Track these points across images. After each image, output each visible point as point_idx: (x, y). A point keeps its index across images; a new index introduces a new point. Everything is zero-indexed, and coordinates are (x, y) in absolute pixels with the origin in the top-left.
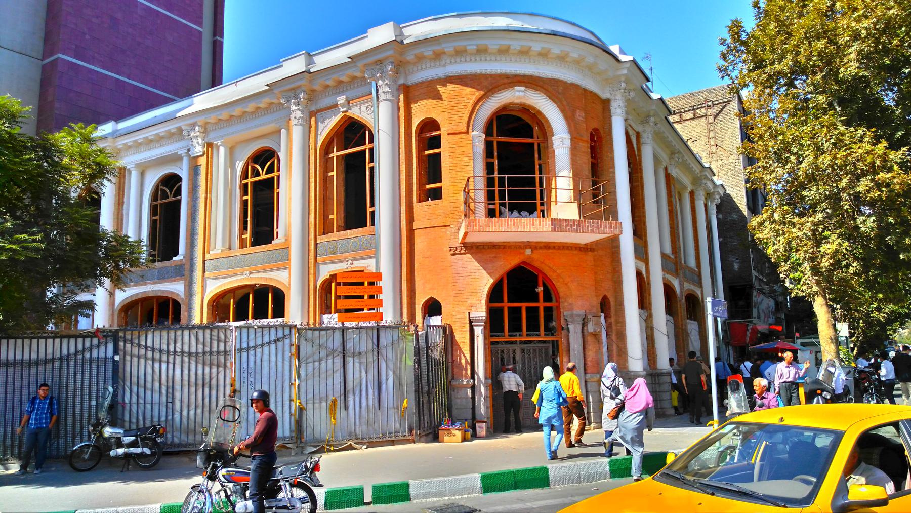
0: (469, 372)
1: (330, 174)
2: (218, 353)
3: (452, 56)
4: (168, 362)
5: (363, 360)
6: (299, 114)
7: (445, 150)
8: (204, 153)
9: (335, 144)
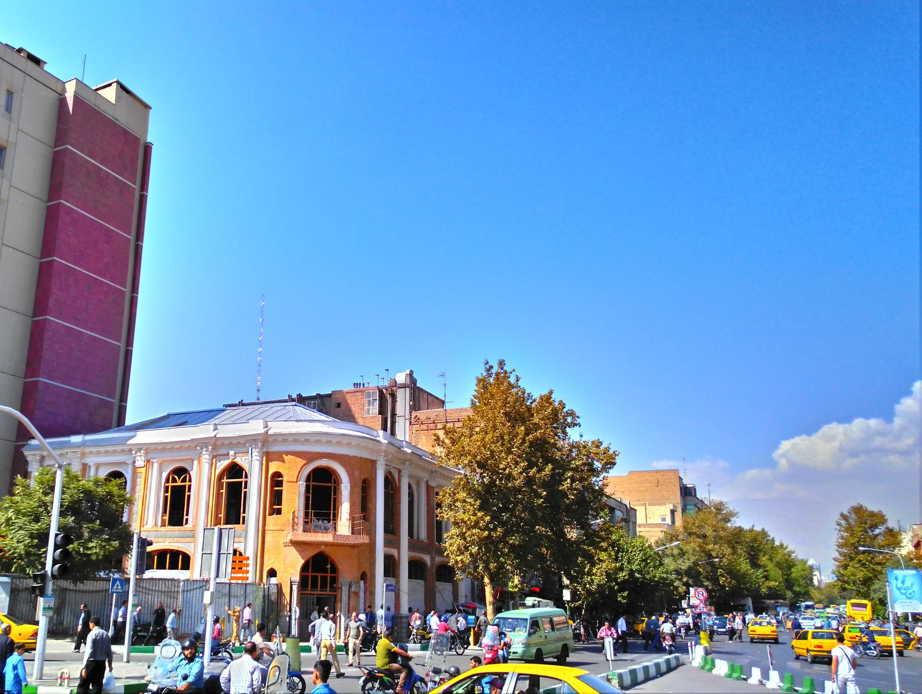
0: (288, 608)
1: (221, 491)
2: (174, 592)
4: (152, 595)
5: (238, 599)
6: (207, 457)
7: (285, 489)
8: (145, 466)
9: (225, 474)
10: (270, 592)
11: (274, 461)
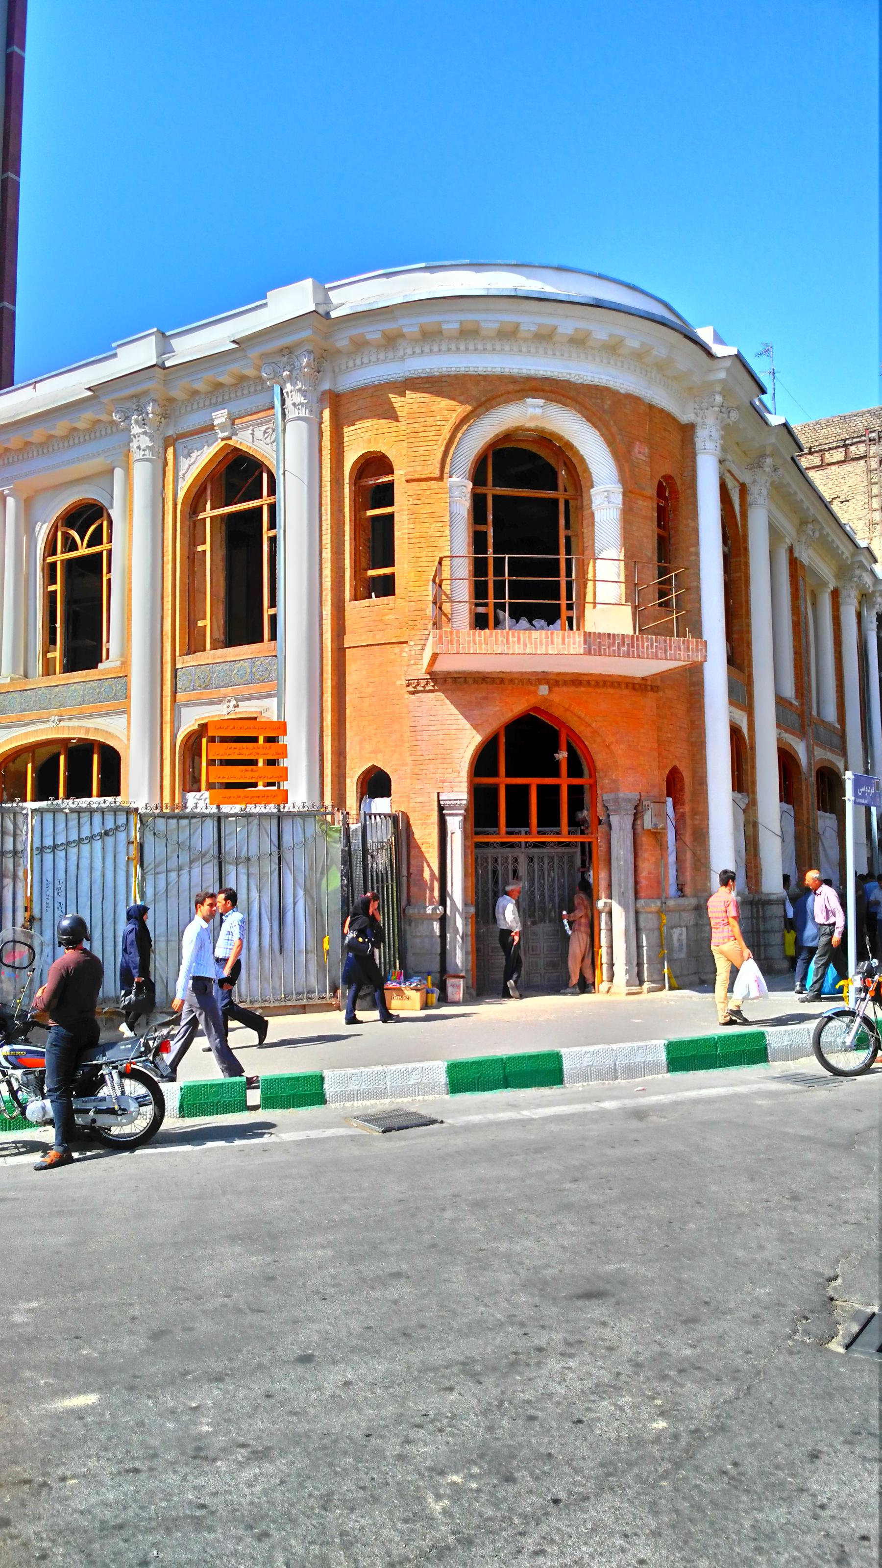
0: (436, 894)
1: (200, 548)
3: (416, 341)
6: (145, 441)
10: (369, 841)
11: (361, 419)
